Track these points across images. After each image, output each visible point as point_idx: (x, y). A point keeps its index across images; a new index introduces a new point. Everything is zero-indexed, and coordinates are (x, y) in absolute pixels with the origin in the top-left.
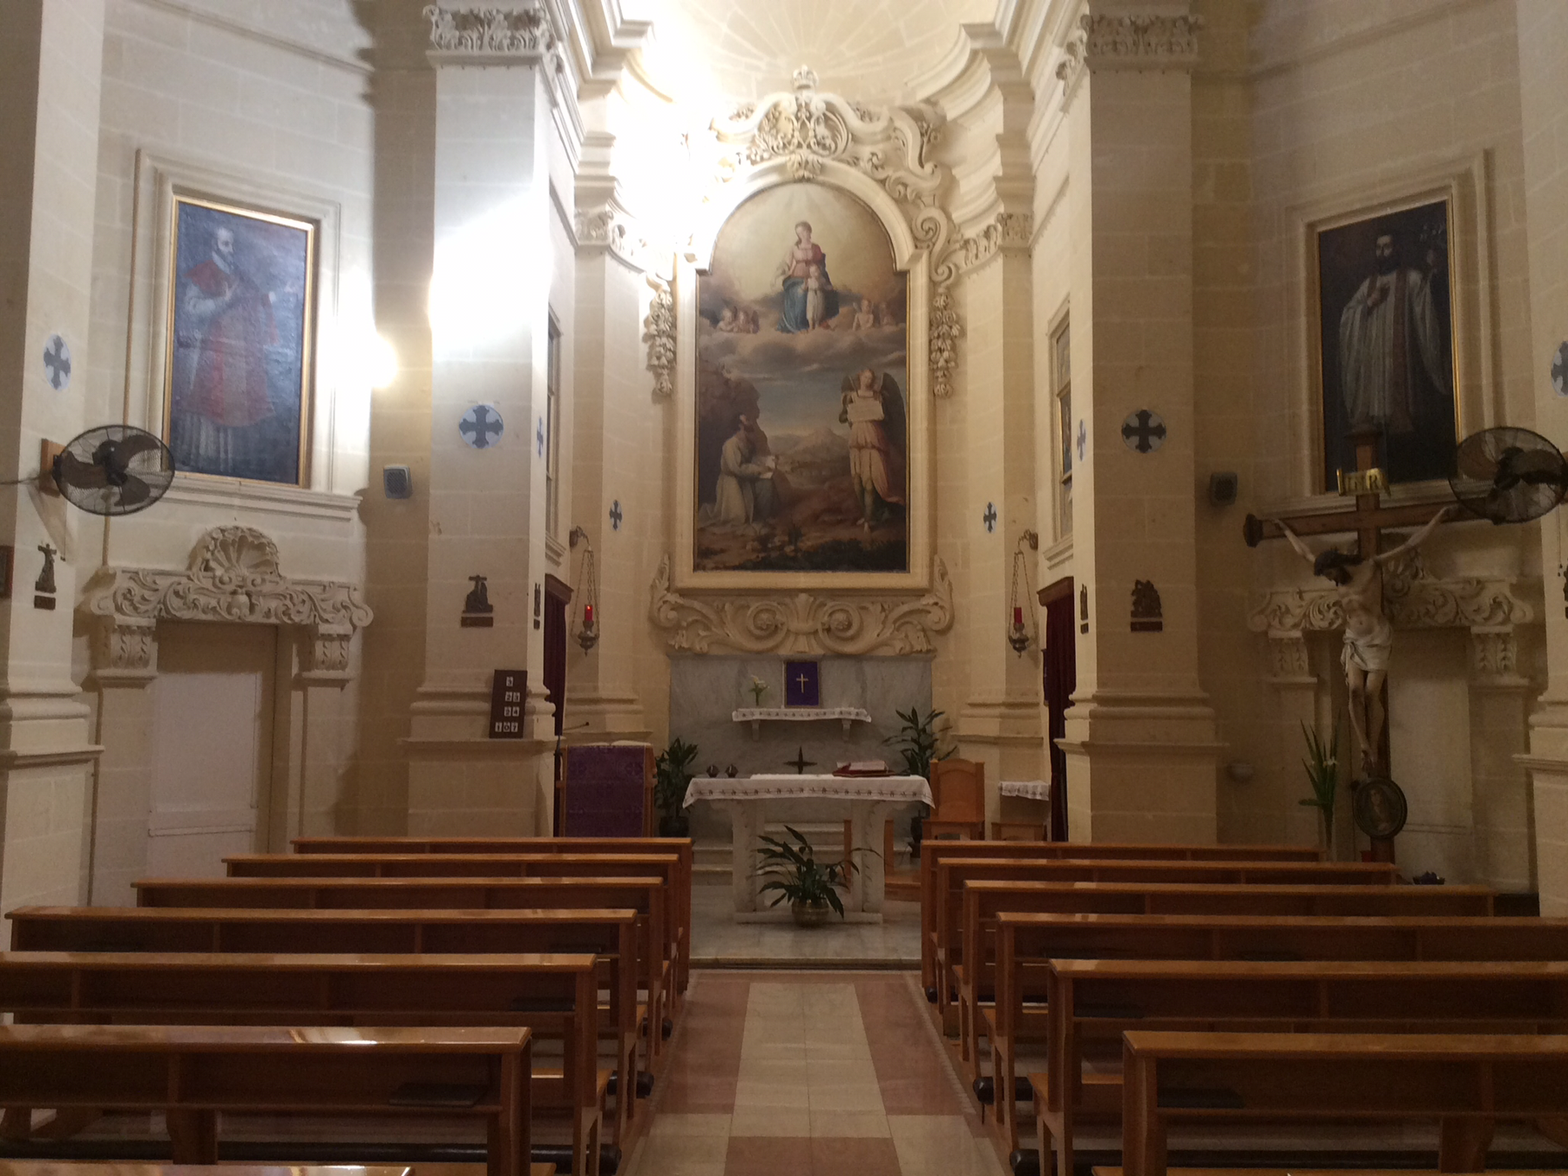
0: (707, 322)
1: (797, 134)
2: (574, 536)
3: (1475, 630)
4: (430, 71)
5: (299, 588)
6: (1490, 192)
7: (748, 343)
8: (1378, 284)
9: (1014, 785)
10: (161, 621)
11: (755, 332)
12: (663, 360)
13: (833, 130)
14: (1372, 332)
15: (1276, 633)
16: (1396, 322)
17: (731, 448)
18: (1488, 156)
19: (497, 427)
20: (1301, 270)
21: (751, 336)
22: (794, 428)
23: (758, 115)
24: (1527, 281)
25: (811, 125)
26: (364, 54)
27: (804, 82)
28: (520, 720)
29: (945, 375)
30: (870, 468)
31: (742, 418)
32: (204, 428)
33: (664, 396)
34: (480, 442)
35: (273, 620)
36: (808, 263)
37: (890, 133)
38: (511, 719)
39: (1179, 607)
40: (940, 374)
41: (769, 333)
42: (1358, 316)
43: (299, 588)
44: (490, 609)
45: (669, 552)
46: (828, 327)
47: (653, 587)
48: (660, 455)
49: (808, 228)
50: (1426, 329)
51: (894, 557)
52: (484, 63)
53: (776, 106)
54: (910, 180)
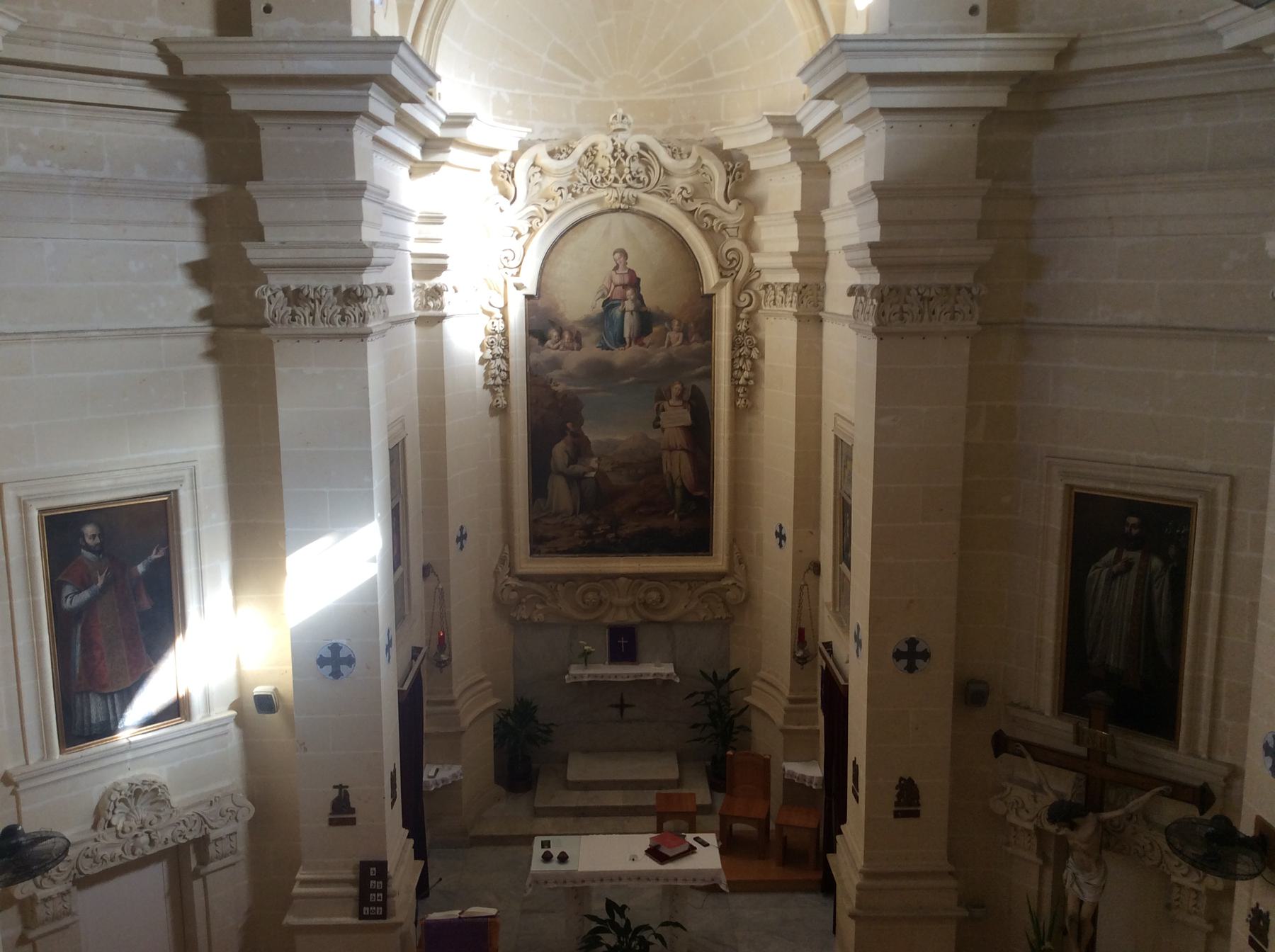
0: (536, 341)
1: (613, 170)
2: (427, 571)
3: (1174, 879)
4: (267, 346)
6: (1230, 516)
7: (573, 359)
8: (1124, 556)
9: (797, 768)
11: (579, 349)
12: (499, 381)
13: (647, 165)
15: (1012, 818)
17: (560, 451)
18: (1233, 482)
19: (350, 661)
20: (1054, 522)
21: (576, 352)
22: (611, 433)
23: (580, 149)
24: (1255, 605)
25: (626, 163)
26: (203, 314)
27: (620, 126)
28: (384, 904)
30: (679, 467)
31: (569, 425)
33: (500, 411)
34: (336, 674)
35: (171, 844)
36: (625, 286)
37: (699, 167)
38: (376, 904)
39: (935, 800)
40: (740, 390)
41: (591, 350)
42: (1104, 576)
43: (190, 813)
44: (353, 811)
45: (508, 540)
46: (642, 345)
47: (496, 573)
48: (498, 460)
49: (624, 254)
51: (700, 543)
52: (318, 337)
53: (594, 146)
54: (716, 212)
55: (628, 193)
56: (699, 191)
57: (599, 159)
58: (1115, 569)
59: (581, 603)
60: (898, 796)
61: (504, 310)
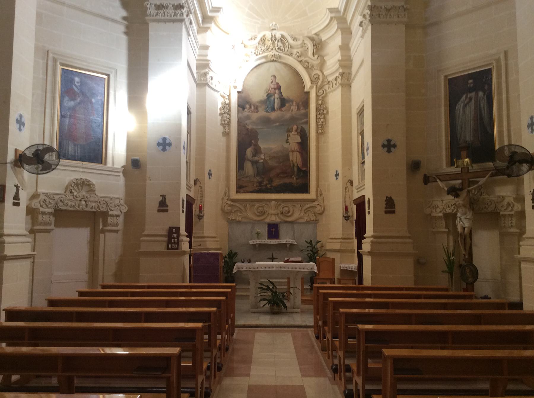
0: (241, 109)
1: (271, 45)
3: (501, 213)
5: (103, 199)
7: (255, 116)
10: (56, 210)
11: (257, 112)
12: (226, 122)
13: (284, 44)
14: (466, 112)
15: (434, 214)
16: (475, 109)
17: (249, 152)
18: (506, 53)
19: (170, 144)
21: (256, 114)
22: (270, 145)
23: (258, 39)
25: (276, 42)
26: (125, 18)
27: (274, 28)
28: (178, 244)
29: (322, 127)
30: (296, 158)
31: (253, 141)
32: (70, 145)
33: (226, 134)
34: (164, 150)
36: (275, 89)
37: (303, 45)
38: (174, 243)
40: (320, 126)
41: (262, 113)
42: (462, 107)
43: (103, 199)
44: (167, 206)
45: (228, 187)
46: (282, 111)
47: (222, 199)
48: (225, 154)
50: (485, 112)
51: (304, 188)
53: (264, 36)
54: (310, 61)
55: (276, 53)
56: (303, 54)
57: (267, 42)
58: (466, 102)
59: (258, 214)
60: (386, 204)
61: (229, 96)
